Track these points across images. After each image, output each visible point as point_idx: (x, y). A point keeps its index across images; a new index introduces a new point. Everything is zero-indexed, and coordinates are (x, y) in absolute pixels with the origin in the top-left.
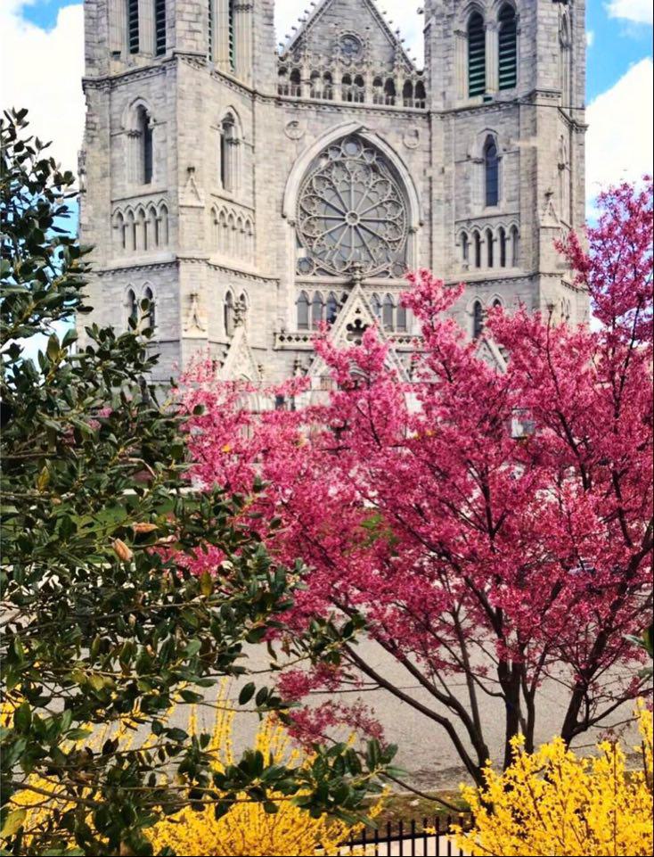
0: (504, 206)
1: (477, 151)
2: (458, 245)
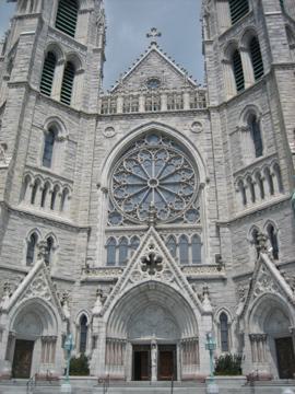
1: (243, 124)
2: (237, 191)
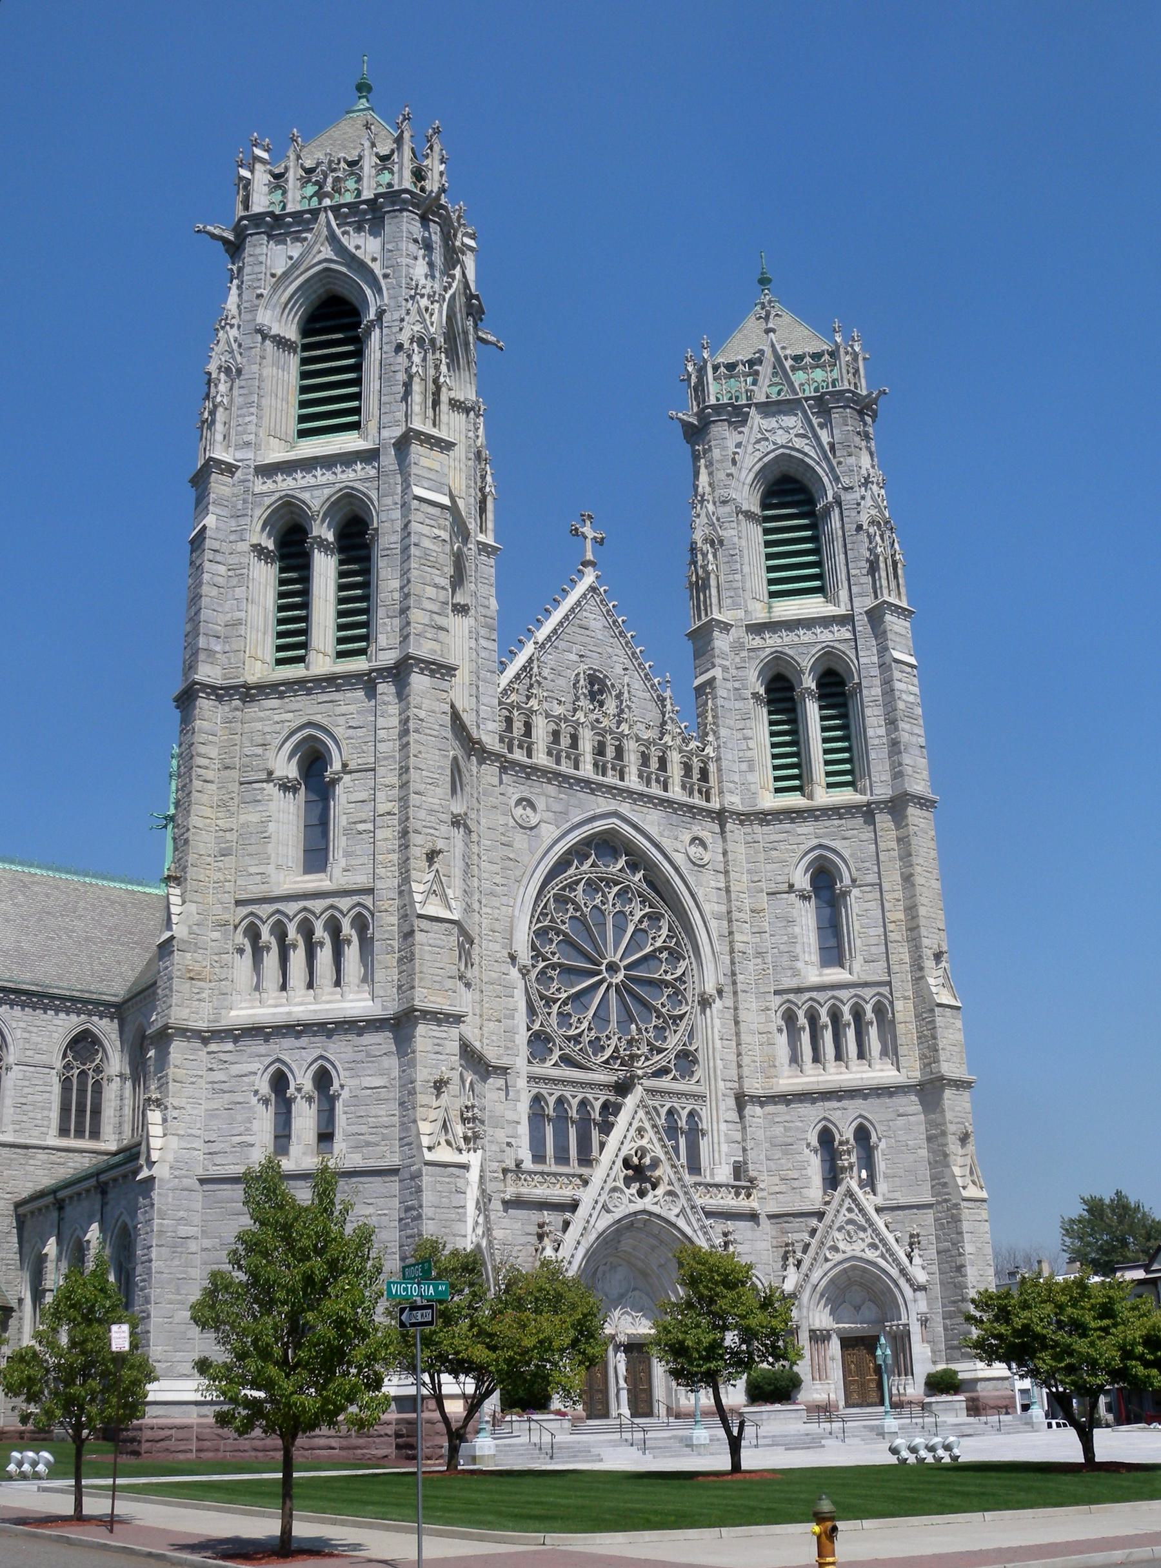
0: (858, 969)
